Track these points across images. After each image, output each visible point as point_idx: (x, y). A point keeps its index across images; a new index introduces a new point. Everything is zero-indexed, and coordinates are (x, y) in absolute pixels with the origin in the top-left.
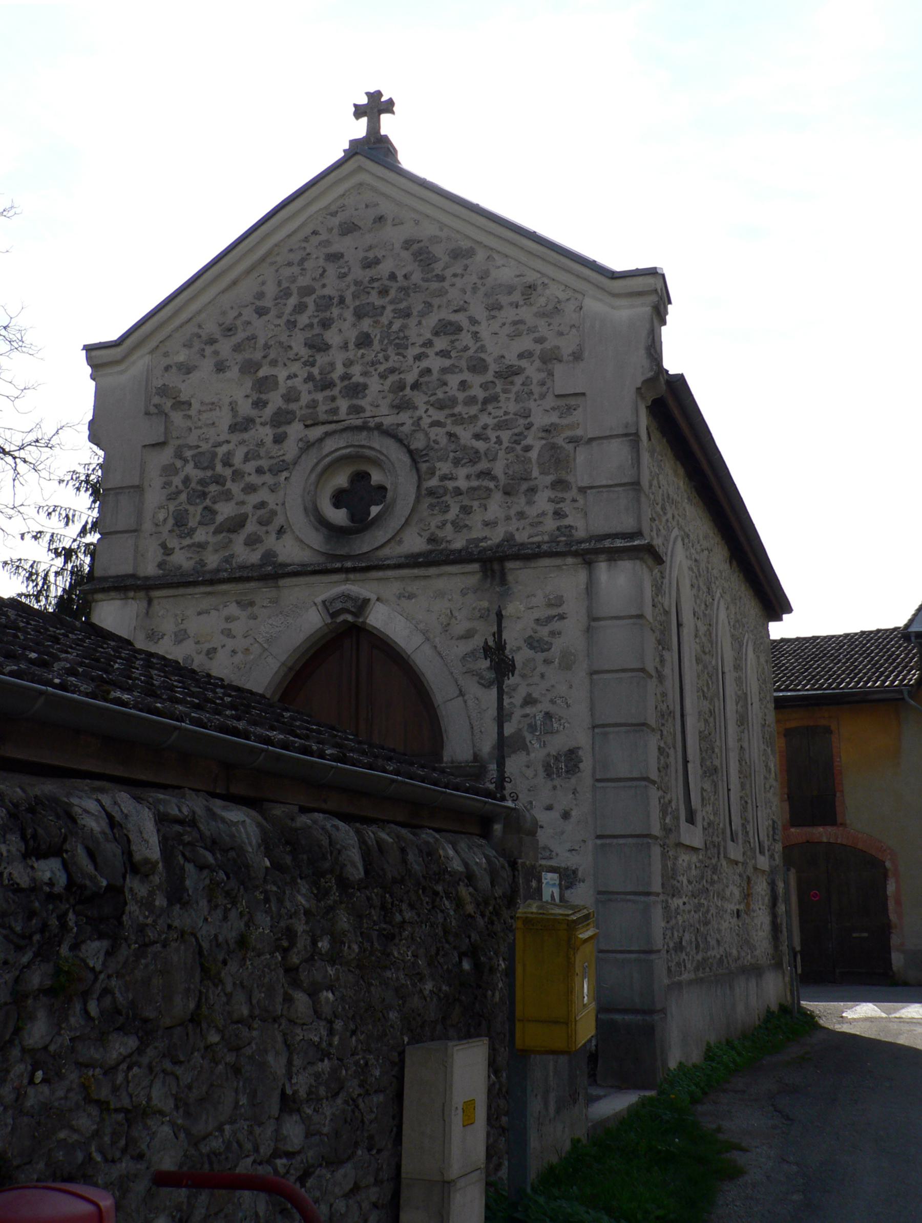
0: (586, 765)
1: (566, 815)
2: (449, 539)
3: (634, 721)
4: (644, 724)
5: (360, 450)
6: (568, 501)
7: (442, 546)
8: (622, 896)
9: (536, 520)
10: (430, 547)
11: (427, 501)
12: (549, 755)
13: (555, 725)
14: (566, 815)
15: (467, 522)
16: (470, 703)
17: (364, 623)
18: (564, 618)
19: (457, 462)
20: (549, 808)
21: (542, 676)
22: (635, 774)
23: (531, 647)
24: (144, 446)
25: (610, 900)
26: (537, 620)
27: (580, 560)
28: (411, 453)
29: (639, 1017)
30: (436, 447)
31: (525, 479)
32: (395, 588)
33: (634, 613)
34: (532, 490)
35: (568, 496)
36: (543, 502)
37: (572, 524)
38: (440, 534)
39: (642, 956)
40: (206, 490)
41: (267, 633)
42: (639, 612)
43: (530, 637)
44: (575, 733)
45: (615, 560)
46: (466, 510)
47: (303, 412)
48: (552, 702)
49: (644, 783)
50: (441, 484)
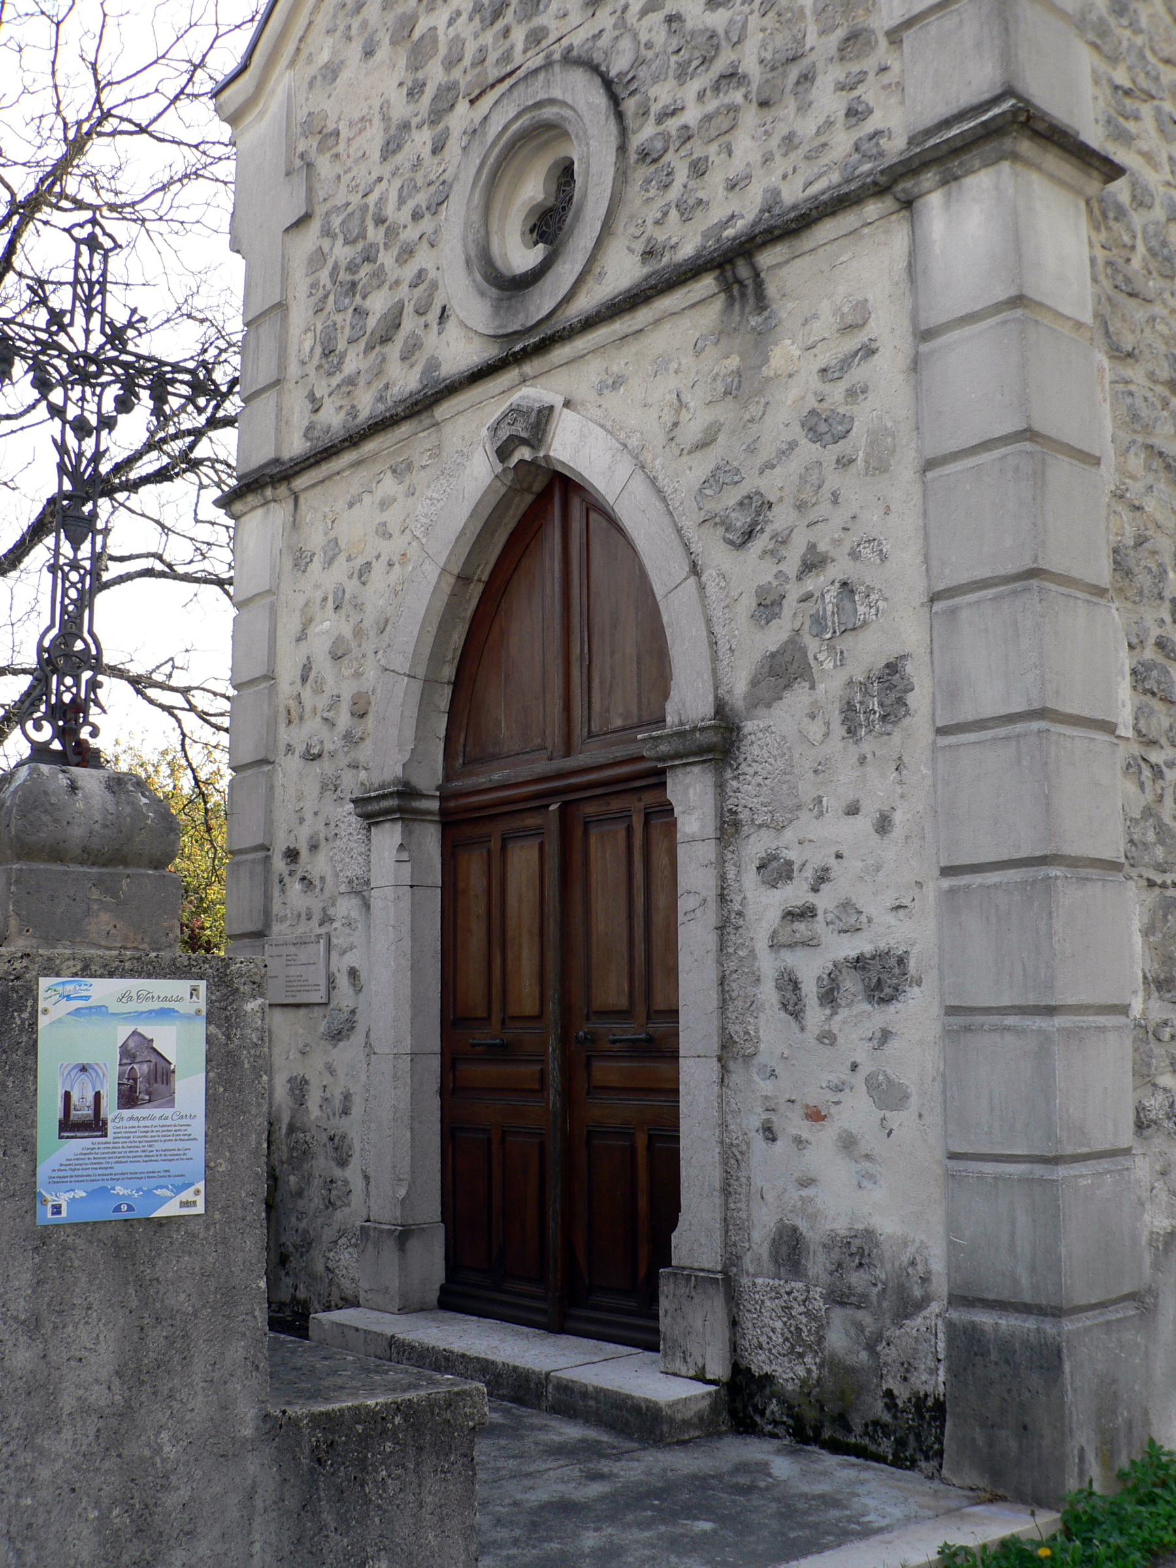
0: (919, 700)
1: (883, 825)
2: (674, 240)
3: (1011, 568)
4: (1033, 573)
5: (536, 113)
6: (871, 76)
7: (665, 260)
8: (994, 1019)
9: (816, 143)
10: (647, 270)
11: (641, 173)
12: (850, 683)
13: (861, 610)
14: (883, 825)
15: (700, 194)
16: (711, 589)
17: (547, 457)
18: (873, 352)
19: (683, 75)
20: (853, 810)
21: (835, 498)
22: (1018, 706)
23: (816, 436)
24: (287, 230)
25: (968, 1029)
26: (825, 370)
27: (888, 203)
28: (608, 84)
29: (1030, 1324)
30: (650, 54)
31: (794, 59)
32: (593, 371)
33: (1003, 296)
34: (806, 77)
35: (869, 64)
36: (827, 100)
37: (880, 126)
38: (661, 236)
39: (1039, 1170)
40: (356, 278)
41: (426, 516)
42: (1013, 292)
43: (813, 412)
44: (898, 627)
45: (956, 178)
46: (699, 169)
47: (468, 78)
48: (854, 555)
49: (1035, 725)
50: (660, 128)
